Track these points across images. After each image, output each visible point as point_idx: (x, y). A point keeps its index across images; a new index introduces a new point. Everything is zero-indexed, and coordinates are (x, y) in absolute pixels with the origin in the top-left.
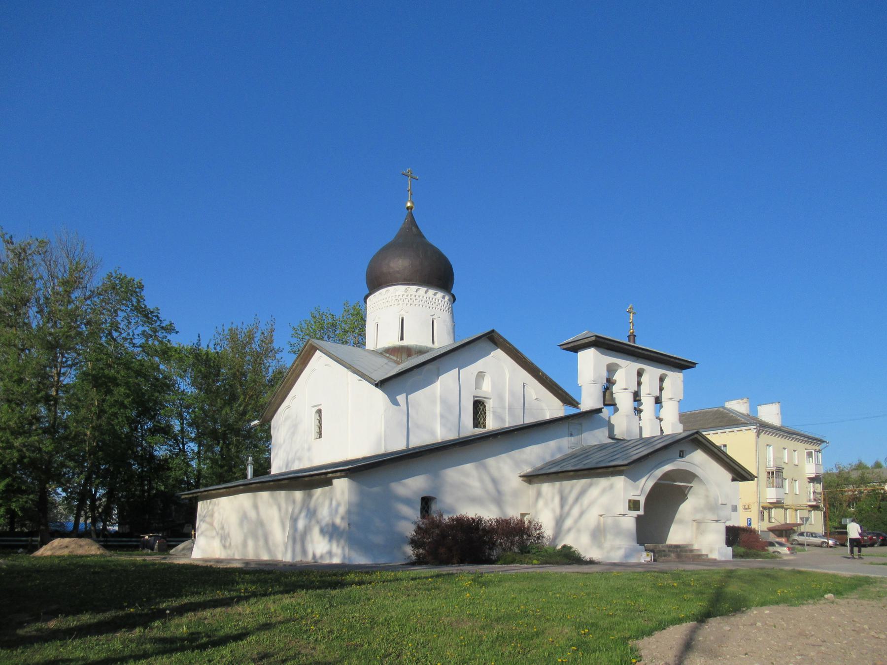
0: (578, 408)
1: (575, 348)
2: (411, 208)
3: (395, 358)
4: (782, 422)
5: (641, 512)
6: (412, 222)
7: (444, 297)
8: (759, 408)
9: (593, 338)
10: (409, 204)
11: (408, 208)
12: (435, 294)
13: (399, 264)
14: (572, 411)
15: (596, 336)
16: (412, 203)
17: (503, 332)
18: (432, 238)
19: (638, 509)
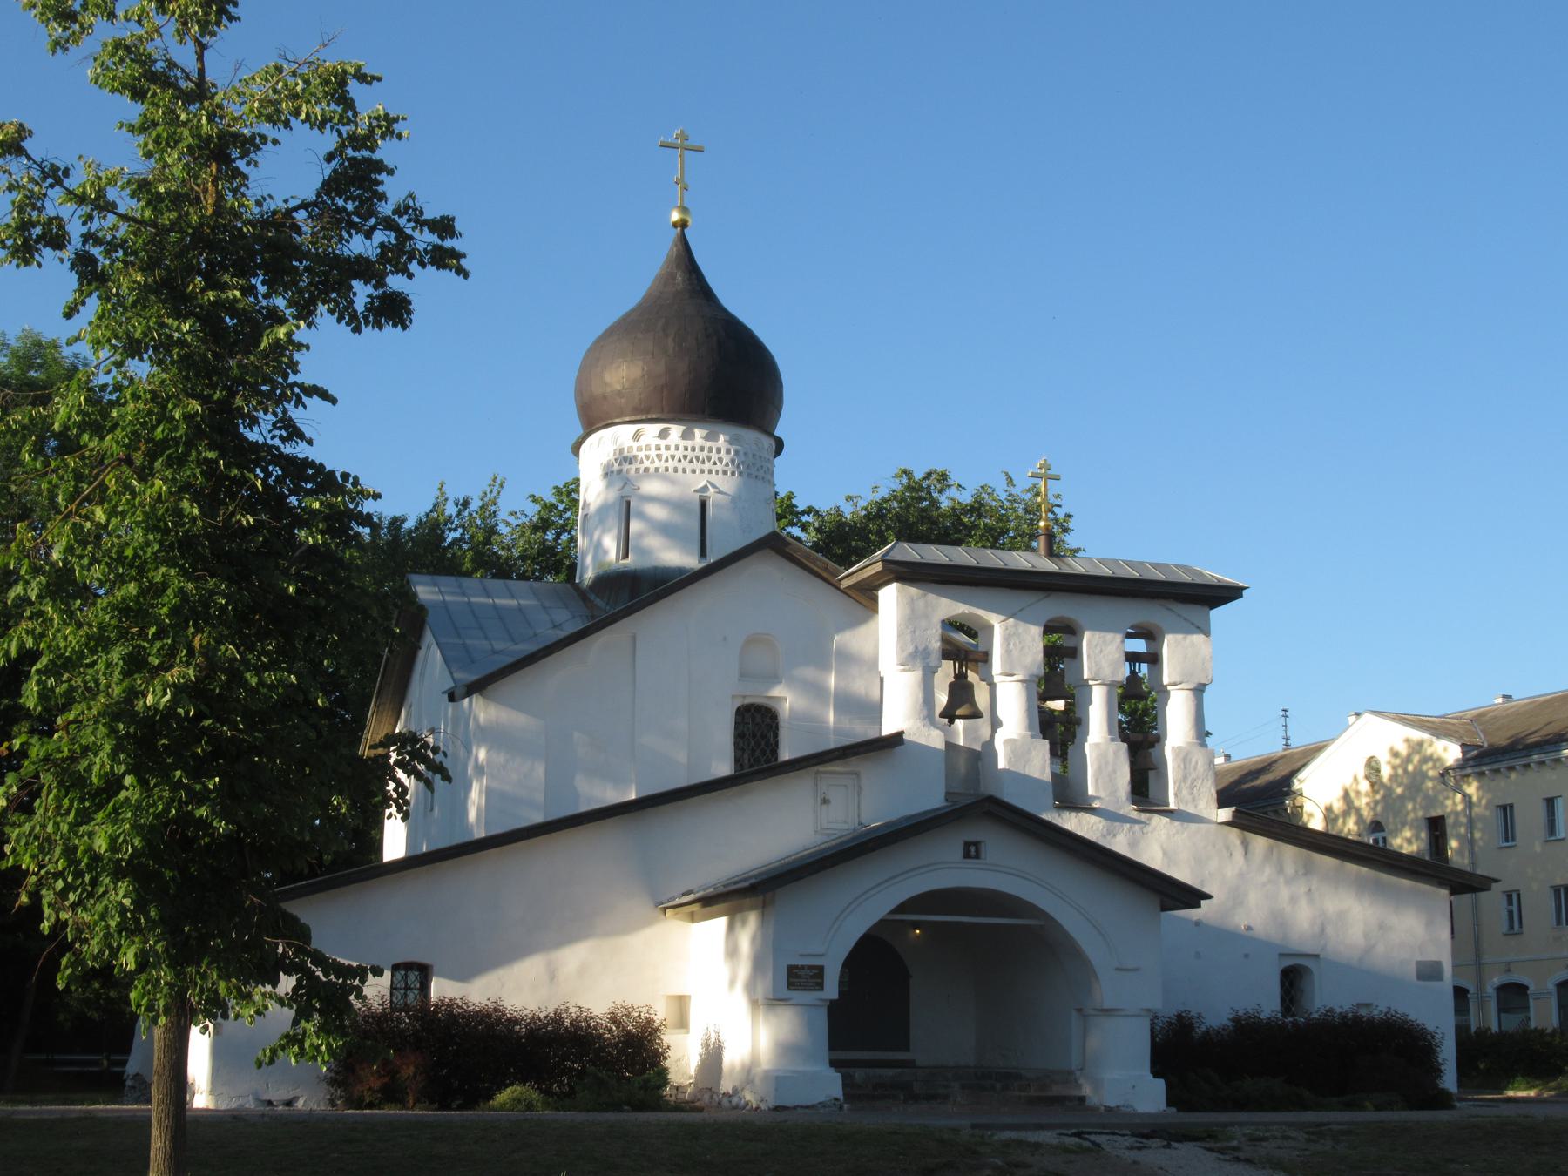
2: (683, 224)
7: (686, 436)
10: (675, 216)
11: (675, 225)
12: (663, 434)
16: (684, 210)
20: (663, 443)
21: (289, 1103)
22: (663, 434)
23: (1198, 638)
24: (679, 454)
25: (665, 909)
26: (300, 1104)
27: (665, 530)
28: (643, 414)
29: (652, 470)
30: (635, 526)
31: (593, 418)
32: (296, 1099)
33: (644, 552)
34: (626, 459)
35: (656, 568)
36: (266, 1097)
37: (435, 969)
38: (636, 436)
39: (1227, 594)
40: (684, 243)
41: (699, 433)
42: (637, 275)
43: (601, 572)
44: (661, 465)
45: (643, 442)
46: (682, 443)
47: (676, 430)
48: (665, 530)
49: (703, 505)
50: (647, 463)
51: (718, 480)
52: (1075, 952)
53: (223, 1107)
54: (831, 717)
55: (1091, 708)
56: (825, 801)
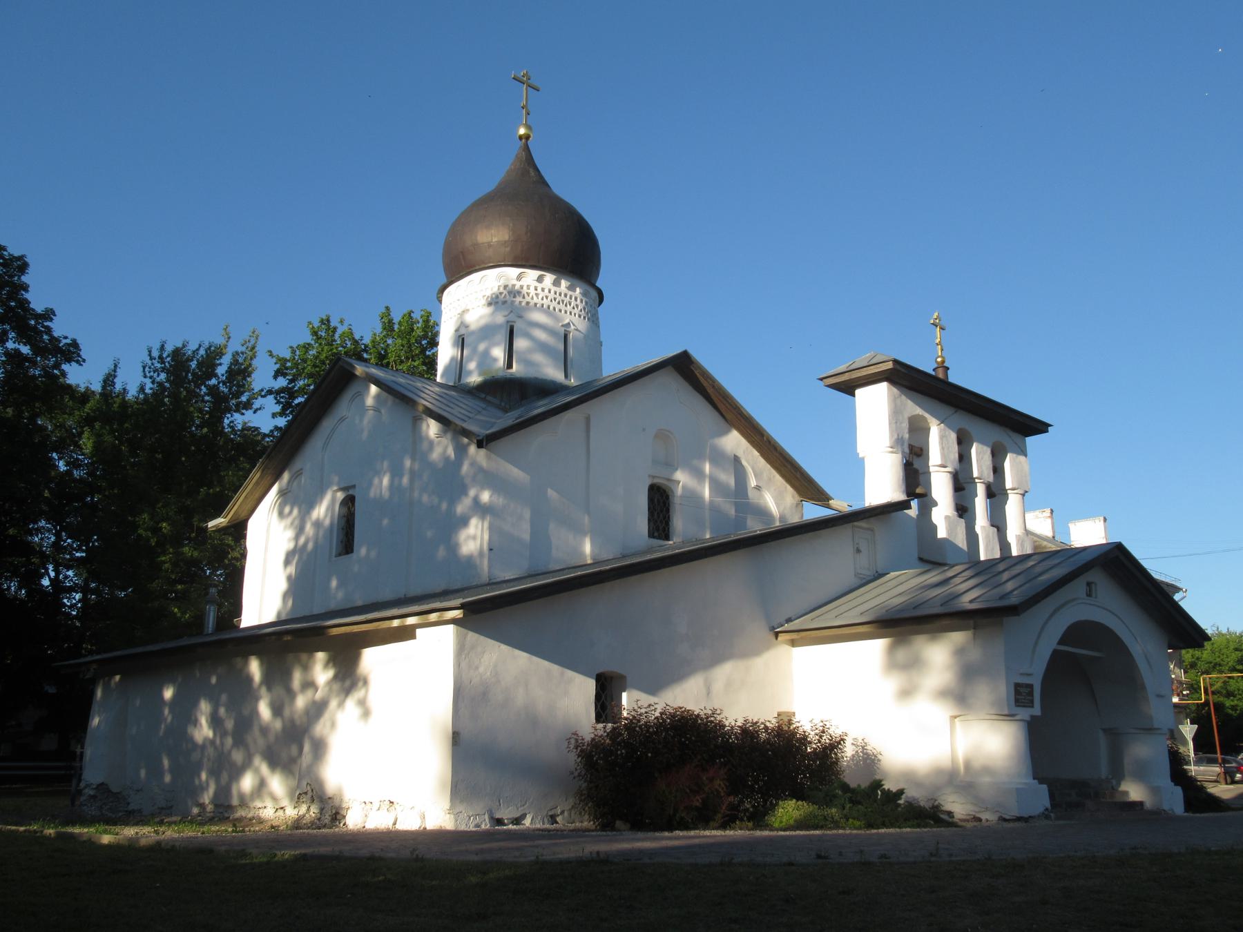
0: (829, 507)
1: (848, 388)
2: (527, 137)
3: (496, 401)
4: (1025, 442)
5: (1037, 710)
6: (528, 160)
7: (556, 283)
8: (1071, 526)
9: (890, 365)
10: (522, 131)
11: (521, 138)
12: (540, 279)
13: (493, 235)
14: (813, 512)
15: (896, 362)
16: (528, 127)
17: (705, 359)
18: (564, 187)
19: (1030, 704)
20: (540, 286)
21: (517, 821)
22: (540, 279)
23: (1022, 458)
24: (552, 296)
25: (777, 635)
26: (527, 822)
27: (544, 348)
28: (522, 261)
29: (532, 304)
30: (520, 344)
31: (459, 265)
32: (524, 816)
33: (527, 363)
34: (514, 293)
35: (536, 379)
36: (498, 816)
37: (629, 679)
38: (519, 278)
39: (1036, 427)
40: (527, 149)
41: (564, 283)
42: (496, 169)
43: (488, 377)
44: (539, 302)
45: (524, 282)
46: (554, 289)
47: (549, 278)
48: (544, 348)
49: (566, 337)
50: (528, 299)
51: (575, 319)
52: (1143, 687)
53: (463, 828)
54: (707, 493)
55: (977, 500)
56: (858, 551)
